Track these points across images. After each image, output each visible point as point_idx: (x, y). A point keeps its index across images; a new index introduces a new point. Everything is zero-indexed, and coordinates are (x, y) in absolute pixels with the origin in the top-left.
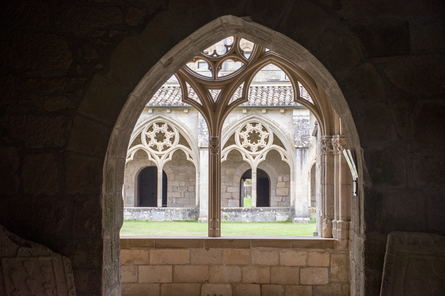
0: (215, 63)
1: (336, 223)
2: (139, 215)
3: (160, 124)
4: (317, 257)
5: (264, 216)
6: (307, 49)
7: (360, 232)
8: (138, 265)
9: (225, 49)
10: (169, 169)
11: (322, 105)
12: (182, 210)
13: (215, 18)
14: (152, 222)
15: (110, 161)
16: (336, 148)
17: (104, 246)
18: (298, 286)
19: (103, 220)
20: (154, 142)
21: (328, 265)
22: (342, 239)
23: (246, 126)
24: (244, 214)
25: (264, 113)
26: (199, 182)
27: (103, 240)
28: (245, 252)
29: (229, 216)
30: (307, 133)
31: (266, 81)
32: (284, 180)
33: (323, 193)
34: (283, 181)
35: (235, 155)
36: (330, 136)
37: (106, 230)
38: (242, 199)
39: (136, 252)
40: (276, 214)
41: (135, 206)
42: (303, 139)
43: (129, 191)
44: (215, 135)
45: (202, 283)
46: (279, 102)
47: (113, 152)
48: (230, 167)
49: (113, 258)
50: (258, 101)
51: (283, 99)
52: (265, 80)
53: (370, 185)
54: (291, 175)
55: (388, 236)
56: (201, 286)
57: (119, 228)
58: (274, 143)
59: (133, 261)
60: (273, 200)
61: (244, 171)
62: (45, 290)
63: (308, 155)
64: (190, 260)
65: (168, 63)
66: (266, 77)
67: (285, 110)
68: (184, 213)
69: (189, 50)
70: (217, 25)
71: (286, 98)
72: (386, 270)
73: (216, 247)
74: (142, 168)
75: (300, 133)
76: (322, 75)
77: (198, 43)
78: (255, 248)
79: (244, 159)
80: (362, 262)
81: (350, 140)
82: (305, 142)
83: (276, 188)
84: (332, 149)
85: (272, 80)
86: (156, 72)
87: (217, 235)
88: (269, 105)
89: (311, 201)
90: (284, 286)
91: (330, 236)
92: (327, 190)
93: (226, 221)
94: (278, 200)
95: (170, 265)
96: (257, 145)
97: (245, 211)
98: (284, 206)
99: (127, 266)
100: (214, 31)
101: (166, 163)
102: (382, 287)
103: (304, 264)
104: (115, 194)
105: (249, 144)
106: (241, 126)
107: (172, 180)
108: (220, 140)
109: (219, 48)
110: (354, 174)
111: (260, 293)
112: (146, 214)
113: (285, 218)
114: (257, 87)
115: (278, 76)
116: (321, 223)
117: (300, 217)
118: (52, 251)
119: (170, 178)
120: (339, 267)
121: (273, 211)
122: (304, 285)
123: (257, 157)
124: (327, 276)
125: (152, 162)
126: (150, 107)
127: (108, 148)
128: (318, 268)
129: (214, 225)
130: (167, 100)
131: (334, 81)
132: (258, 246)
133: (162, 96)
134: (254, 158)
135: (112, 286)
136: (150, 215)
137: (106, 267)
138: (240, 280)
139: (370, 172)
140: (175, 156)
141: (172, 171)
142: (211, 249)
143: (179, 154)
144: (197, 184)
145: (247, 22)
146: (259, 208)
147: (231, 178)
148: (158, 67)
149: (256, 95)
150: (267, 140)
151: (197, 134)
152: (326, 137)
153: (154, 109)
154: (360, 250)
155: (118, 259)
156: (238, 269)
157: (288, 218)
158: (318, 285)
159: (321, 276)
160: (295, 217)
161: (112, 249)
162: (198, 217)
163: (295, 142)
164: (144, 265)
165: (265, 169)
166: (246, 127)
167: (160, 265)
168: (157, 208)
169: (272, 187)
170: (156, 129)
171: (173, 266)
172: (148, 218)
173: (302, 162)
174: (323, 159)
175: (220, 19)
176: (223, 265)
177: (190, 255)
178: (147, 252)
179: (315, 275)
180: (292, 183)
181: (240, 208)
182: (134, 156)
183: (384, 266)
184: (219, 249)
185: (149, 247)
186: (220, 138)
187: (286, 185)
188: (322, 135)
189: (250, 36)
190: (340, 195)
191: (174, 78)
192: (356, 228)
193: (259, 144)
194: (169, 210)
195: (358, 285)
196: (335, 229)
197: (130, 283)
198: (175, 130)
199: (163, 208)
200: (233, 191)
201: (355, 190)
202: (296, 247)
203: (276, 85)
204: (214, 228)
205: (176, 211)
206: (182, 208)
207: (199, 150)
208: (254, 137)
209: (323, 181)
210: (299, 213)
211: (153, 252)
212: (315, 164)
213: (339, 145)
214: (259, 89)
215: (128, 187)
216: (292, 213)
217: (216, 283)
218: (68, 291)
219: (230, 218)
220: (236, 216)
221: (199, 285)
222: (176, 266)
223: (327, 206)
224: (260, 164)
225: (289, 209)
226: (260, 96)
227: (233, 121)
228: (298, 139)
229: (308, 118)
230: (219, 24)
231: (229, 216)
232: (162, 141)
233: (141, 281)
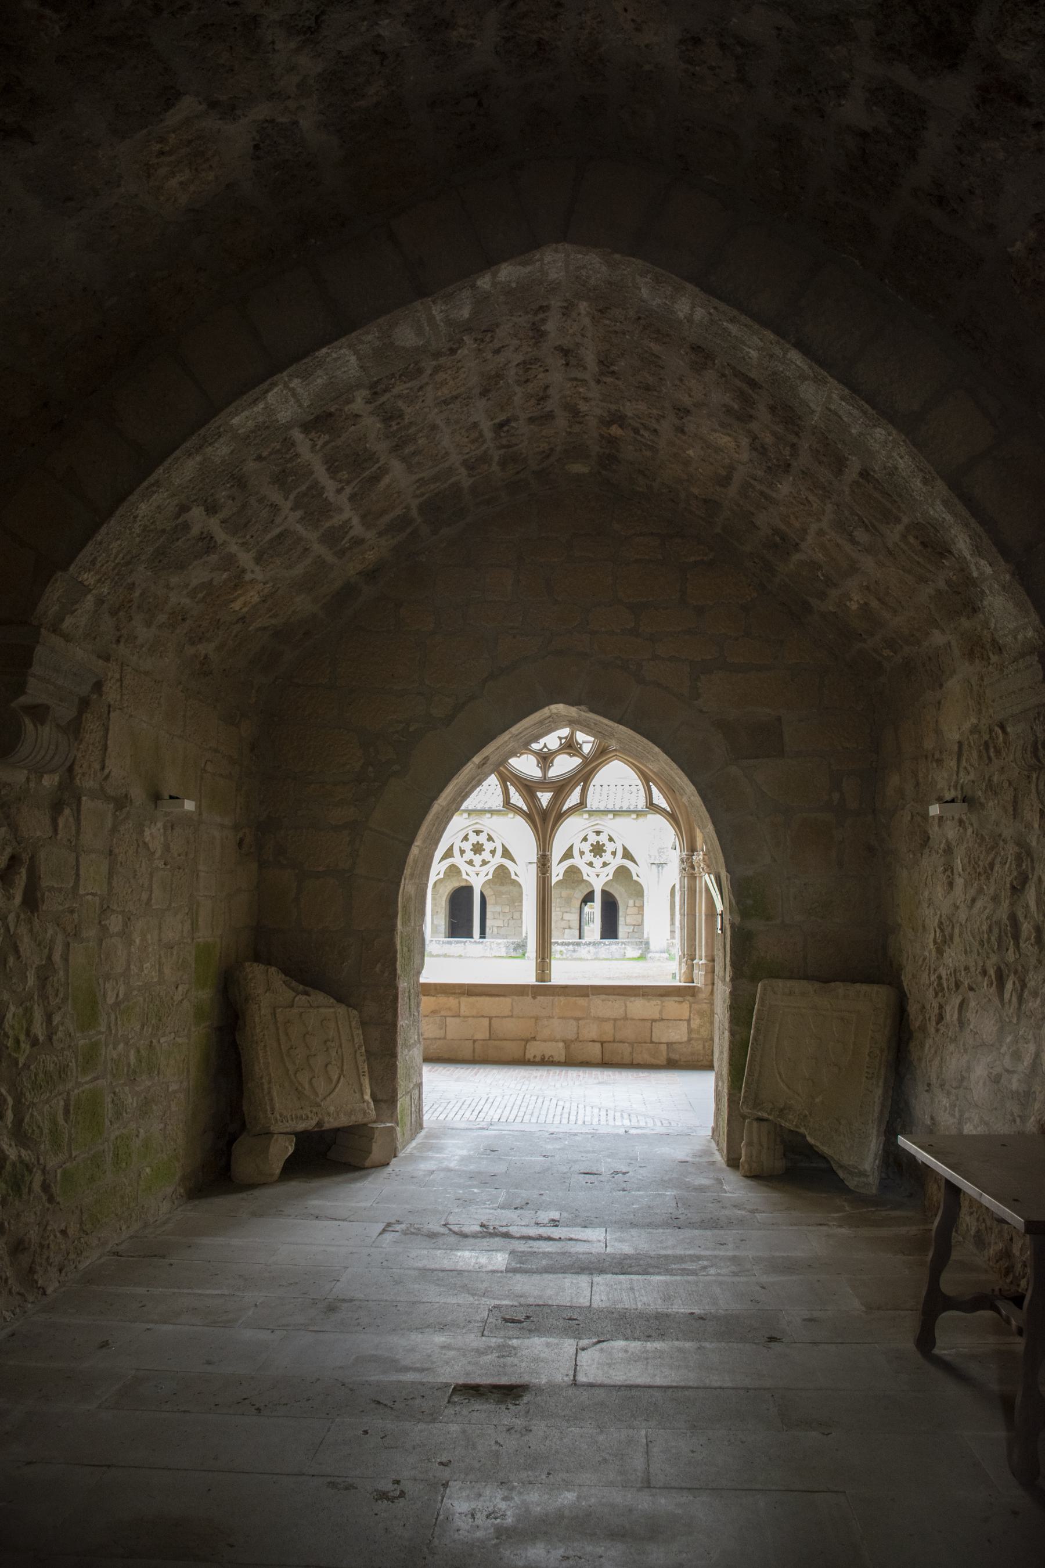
0: (545, 759)
4: (674, 1007)
13: (543, 707)
15: (407, 887)
20: (469, 855)
22: (706, 985)
28: (582, 1001)
39: (443, 1000)
43: (434, 918)
44: (544, 851)
45: (527, 1041)
47: (412, 875)
53: (737, 920)
57: (419, 973)
60: (622, 930)
62: (327, 1050)
64: (512, 1011)
73: (545, 995)
76: (677, 779)
83: (626, 915)
85: (618, 782)
90: (631, 1044)
97: (585, 944)
100: (541, 722)
103: (657, 1016)
104: (414, 929)
109: (552, 741)
110: (719, 907)
113: (637, 953)
126: (465, 811)
129: (543, 966)
131: (693, 788)
137: (402, 1022)
139: (737, 903)
147: (568, 901)
150: (614, 853)
153: (470, 812)
154: (724, 1002)
155: (418, 1012)
156: (573, 1022)
165: (611, 891)
167: (473, 1017)
169: (621, 913)
171: (490, 1018)
189: (587, 728)
197: (435, 1039)
201: (719, 927)
208: (598, 850)
211: (465, 1000)
220: (574, 951)
224: (606, 884)
227: (570, 832)
230: (548, 714)
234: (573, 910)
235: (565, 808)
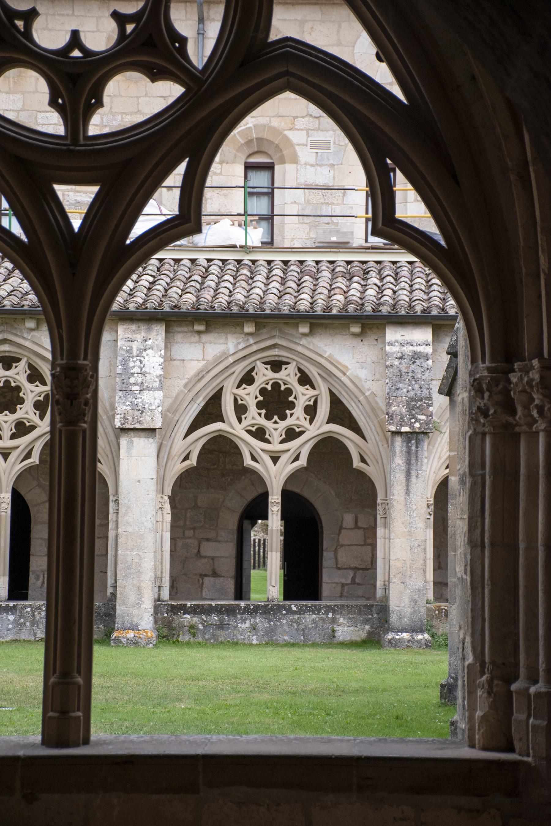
5: (302, 627)
9: (112, 26)
16: (526, 407)
24: (244, 621)
25: (305, 335)
29: (201, 627)
30: (426, 392)
32: (360, 524)
34: (357, 527)
38: (244, 574)
40: (334, 621)
46: (348, 302)
50: (289, 300)
51: (358, 294)
52: (309, 244)
54: (380, 508)
58: (220, 418)
60: (329, 580)
61: (250, 496)
63: (426, 454)
66: (313, 235)
67: (363, 327)
71: (368, 292)
79: (248, 461)
82: (420, 417)
83: (338, 546)
84: (513, 412)
88: (319, 310)
89: (435, 584)
94: (343, 581)
96: (283, 425)
98: (358, 597)
105: (262, 421)
106: (240, 370)
113: (360, 632)
114: (286, 263)
115: (345, 233)
121: (326, 613)
123: (284, 458)
134: (275, 460)
144: (111, 534)
146: (288, 603)
149: (283, 284)
150: (311, 411)
151: (114, 390)
152: (489, 369)
157: (369, 633)
160: (388, 630)
162: (113, 630)
165: (306, 493)
169: (327, 543)
174: (478, 451)
180: (380, 532)
181: (237, 602)
196: (522, 717)
200: (217, 554)
203: (341, 258)
208: (276, 402)
209: (478, 531)
212: (447, 477)
213: (537, 399)
214: (292, 268)
219: (204, 633)
220: (221, 626)
223: (491, 626)
224: (293, 477)
226: (294, 285)
229: (429, 350)
231: (201, 627)
234: (223, 534)
235: (141, 227)
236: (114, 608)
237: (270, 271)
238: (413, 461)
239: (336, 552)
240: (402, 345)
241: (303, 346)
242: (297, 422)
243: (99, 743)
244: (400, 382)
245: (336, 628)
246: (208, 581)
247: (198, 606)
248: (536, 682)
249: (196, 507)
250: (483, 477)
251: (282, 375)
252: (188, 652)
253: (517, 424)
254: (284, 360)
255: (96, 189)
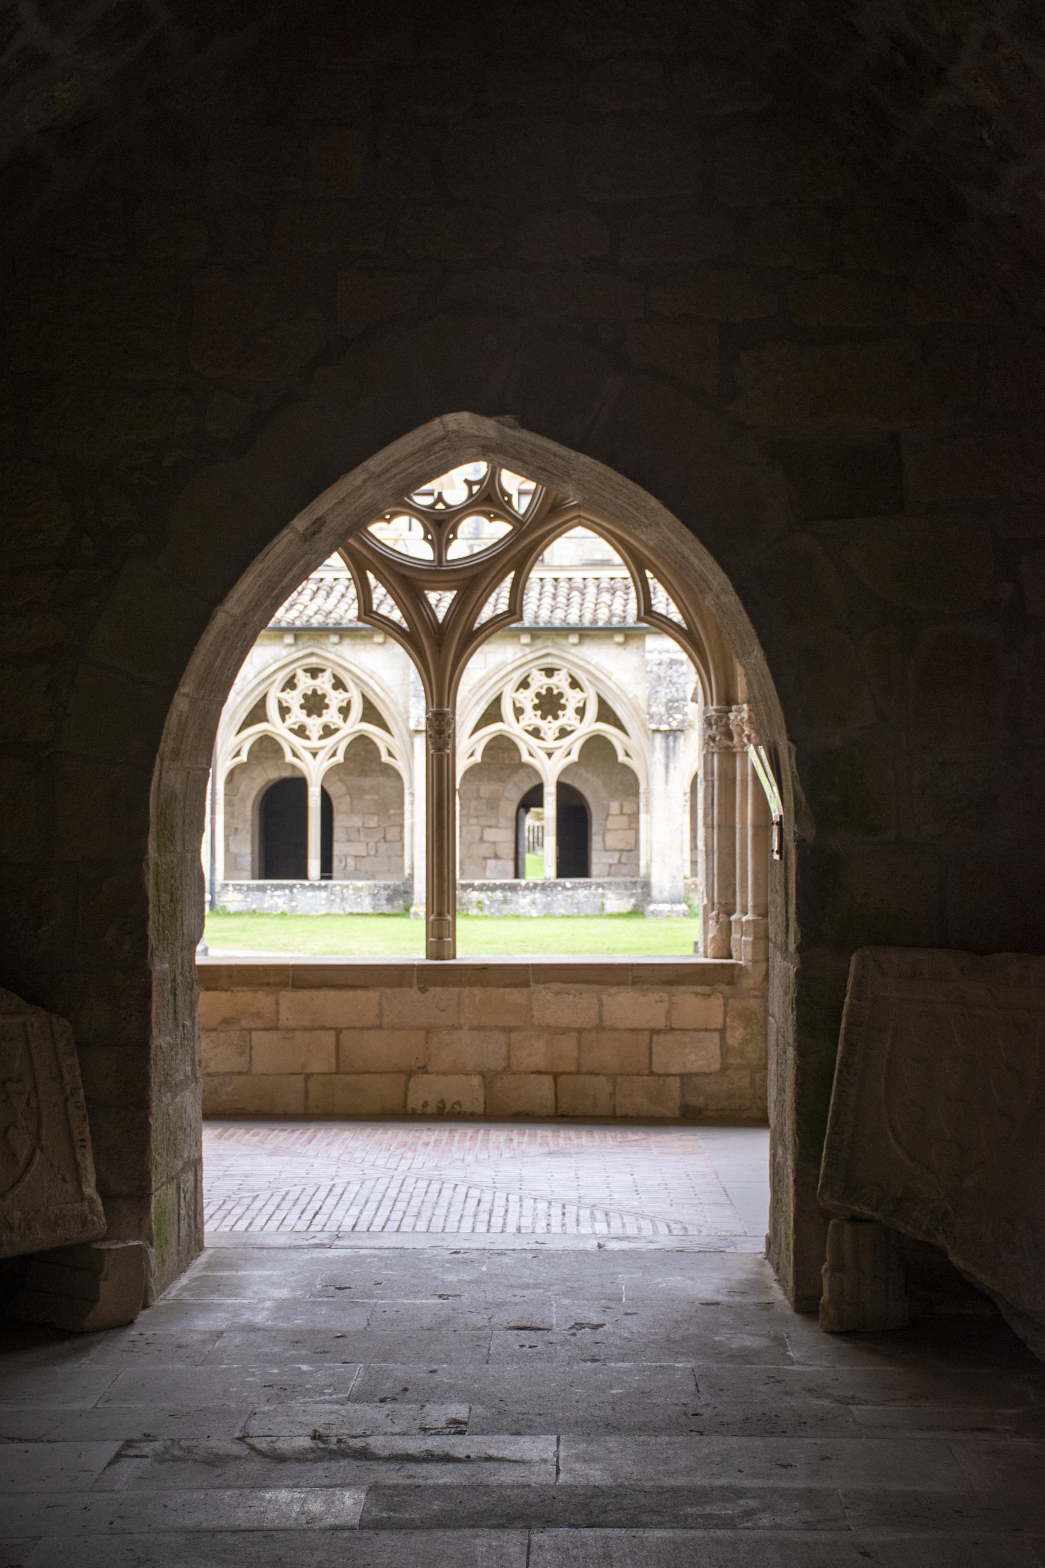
0: (440, 524)
1: (739, 921)
2: (262, 900)
3: (314, 672)
4: (692, 1006)
5: (575, 901)
6: (657, 496)
7: (787, 949)
8: (250, 1030)
9: (465, 489)
10: (339, 784)
11: (707, 632)
12: (370, 887)
14: (295, 916)
15: (167, 775)
16: (740, 735)
17: (154, 989)
18: (645, 1078)
19: (150, 924)
20: (298, 716)
21: (719, 1026)
22: (755, 962)
23: (528, 676)
24: (524, 897)
25: (575, 645)
26: (412, 816)
27: (151, 973)
28: (516, 996)
29: (487, 902)
30: (681, 695)
31: (579, 563)
32: (625, 811)
33: (710, 848)
34: (622, 813)
35: (501, 750)
36: (724, 707)
37: (160, 948)
38: (520, 857)
39: (245, 997)
40: (603, 895)
41: (253, 878)
42: (671, 708)
44: (440, 704)
45: (410, 1074)
46: (612, 615)
48: (489, 779)
49: (179, 1017)
50: (559, 614)
52: (577, 562)
53: (810, 834)
54: (642, 797)
55: (853, 958)
56: (409, 1080)
59: (239, 1020)
60: (598, 860)
61: (527, 787)
63: (682, 748)
64: (380, 1015)
65: (312, 529)
67: (626, 637)
68: (375, 895)
69: (365, 497)
70: (433, 437)
71: (629, 606)
72: (845, 1040)
73: (444, 984)
74: (270, 781)
75: (664, 693)
76: (695, 561)
77: (388, 480)
78: (541, 986)
79: (526, 758)
80: (790, 1022)
81: (765, 722)
83: (605, 831)
84: (731, 738)
85: (581, 566)
86: (282, 553)
87: (446, 954)
88: (586, 623)
90: (612, 1077)
91: (726, 954)
92: (719, 840)
93: (480, 914)
94: (611, 861)
95: (331, 1029)
97: (527, 887)
98: (624, 875)
99: (222, 1031)
100: (426, 450)
101: (331, 769)
102: (835, 1082)
103: (661, 1023)
106: (517, 677)
107: (345, 813)
108: (454, 719)
109: (453, 486)
110: (776, 808)
111: (552, 1097)
112: (279, 896)
113: (627, 905)
114: (556, 580)
116: (705, 923)
117: (664, 902)
118: (24, 1003)
119: (340, 806)
120: (745, 1028)
121: (597, 889)
122: (660, 1075)
124: (718, 1051)
125: (293, 767)
127: (162, 744)
128: (695, 1034)
130: (330, 612)
132: (550, 982)
133: (319, 600)
135: (176, 1085)
136: (291, 900)
137: (161, 1040)
138: (505, 1064)
140: (353, 751)
141: (344, 790)
142: (432, 989)
143: (362, 745)
145: (507, 430)
146: (562, 880)
148: (286, 540)
150: (581, 712)
152: (716, 711)
154: (786, 992)
155: (193, 1019)
156: (499, 1037)
157: (635, 906)
158: (696, 1074)
159: (703, 1052)
161: (175, 996)
162: (411, 905)
163: (651, 717)
164: (265, 1029)
165: (577, 784)
166: (529, 680)
167: (305, 1029)
168: (307, 883)
169: (595, 827)
170: (305, 683)
171: (338, 1031)
172: (285, 907)
173: (667, 767)
174: (709, 764)
175: (441, 422)
176: (460, 1028)
177: (380, 1003)
178: (273, 998)
179: (687, 1051)
180: (643, 817)
182: (250, 752)
183: (842, 1031)
184: (451, 989)
185: (276, 985)
186: (454, 713)
187: (630, 823)
188: (706, 704)
190: (749, 853)
191: (336, 560)
192: (779, 938)
193: (561, 722)
194: (338, 888)
195: (782, 1076)
197: (231, 1073)
198: (350, 685)
199: (324, 883)
200: (498, 839)
202: (643, 983)
204: (440, 938)
205: (353, 890)
206: (371, 882)
207: (411, 737)
208: (550, 704)
209: (710, 817)
210: (661, 892)
211: (287, 997)
215: (236, 829)
216: (643, 893)
217: (444, 1074)
218: (66, 1100)
219: (490, 907)
220: (505, 901)
221: (403, 1078)
222: (345, 1032)
224: (566, 771)
225: (636, 882)
227: (486, 670)
228: (659, 709)
230: (440, 433)
231: (487, 902)
232: (320, 715)
233: (258, 1068)
234: (503, 822)
236: (412, 886)
237: (542, 587)
238: (671, 755)
239: (603, 836)
240: (660, 653)
241: (574, 655)
242: (569, 722)
243: (461, 959)
244: (659, 685)
245: (605, 902)
246: (491, 863)
247: (484, 885)
248: (746, 913)
249: (479, 797)
250: (713, 782)
251: (317, 682)
252: (477, 922)
253: (735, 747)
254: (556, 667)
255: (455, 592)
